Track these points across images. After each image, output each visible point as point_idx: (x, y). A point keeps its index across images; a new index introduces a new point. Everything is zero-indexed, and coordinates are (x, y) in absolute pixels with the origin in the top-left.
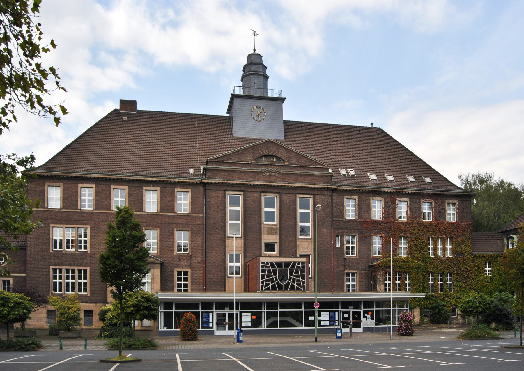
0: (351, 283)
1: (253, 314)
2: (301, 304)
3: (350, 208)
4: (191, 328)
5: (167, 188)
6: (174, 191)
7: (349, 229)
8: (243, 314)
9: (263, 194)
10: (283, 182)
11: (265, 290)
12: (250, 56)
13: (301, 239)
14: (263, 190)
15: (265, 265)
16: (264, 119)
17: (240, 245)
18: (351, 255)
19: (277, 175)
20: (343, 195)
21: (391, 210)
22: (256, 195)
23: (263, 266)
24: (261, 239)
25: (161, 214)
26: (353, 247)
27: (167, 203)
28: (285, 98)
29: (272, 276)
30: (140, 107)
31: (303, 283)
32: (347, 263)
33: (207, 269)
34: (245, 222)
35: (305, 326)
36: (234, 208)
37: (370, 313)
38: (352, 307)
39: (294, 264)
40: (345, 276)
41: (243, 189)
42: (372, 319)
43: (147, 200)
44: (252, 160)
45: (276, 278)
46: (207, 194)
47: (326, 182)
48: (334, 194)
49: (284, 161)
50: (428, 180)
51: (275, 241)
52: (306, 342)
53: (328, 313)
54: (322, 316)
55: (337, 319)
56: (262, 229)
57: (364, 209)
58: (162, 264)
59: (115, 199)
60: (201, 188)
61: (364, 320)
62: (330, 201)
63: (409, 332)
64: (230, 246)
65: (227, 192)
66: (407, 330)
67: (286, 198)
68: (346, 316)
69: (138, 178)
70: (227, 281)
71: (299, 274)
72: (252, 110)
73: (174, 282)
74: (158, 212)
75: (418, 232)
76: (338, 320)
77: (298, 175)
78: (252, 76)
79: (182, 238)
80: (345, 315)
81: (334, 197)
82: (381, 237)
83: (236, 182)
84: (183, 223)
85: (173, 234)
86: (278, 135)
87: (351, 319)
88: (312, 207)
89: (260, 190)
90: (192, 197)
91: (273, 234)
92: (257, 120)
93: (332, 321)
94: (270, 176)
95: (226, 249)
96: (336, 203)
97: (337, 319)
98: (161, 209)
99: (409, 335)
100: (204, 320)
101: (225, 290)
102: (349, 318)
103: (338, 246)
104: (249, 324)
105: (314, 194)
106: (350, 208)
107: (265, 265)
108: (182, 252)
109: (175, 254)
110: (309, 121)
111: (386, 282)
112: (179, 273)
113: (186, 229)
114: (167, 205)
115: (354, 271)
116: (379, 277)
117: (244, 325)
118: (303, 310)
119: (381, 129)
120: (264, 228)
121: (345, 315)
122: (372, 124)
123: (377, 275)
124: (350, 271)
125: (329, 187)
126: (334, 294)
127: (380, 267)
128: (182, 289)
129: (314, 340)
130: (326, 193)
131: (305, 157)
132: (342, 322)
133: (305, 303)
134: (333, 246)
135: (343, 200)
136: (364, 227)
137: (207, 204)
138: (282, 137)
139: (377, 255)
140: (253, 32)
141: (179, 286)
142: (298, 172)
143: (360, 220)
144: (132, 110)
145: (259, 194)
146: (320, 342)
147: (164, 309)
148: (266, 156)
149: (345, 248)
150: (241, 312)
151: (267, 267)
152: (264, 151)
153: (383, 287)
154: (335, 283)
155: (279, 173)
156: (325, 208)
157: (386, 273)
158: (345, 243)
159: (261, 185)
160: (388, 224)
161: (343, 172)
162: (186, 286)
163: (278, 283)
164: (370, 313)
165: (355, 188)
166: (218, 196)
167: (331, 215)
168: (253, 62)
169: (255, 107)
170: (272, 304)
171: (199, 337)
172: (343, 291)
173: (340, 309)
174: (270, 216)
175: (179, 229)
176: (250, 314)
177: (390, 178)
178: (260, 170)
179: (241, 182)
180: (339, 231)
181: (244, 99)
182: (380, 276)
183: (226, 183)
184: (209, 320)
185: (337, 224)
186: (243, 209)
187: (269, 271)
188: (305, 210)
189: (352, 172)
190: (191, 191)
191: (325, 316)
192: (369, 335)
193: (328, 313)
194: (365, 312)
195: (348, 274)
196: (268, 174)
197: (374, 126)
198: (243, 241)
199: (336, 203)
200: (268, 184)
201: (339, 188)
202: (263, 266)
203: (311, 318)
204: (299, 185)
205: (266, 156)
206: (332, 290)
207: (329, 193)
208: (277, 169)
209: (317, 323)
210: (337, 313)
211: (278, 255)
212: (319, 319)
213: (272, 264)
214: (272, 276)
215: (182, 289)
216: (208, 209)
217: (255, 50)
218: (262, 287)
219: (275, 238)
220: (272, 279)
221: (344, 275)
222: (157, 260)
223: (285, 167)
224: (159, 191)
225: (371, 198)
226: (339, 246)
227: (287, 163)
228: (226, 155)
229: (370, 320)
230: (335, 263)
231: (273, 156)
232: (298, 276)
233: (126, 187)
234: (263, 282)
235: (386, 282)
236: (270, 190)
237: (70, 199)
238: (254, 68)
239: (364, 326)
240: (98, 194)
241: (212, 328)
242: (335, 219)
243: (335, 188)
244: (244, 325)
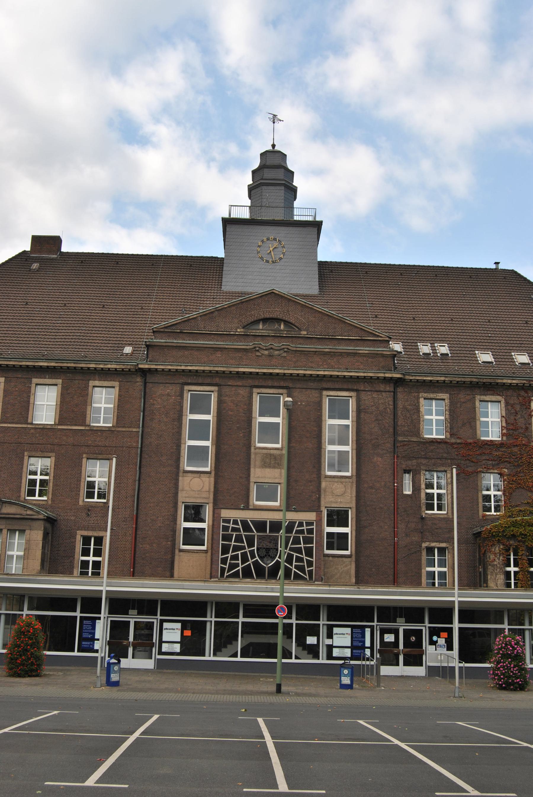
0: (437, 569)
1: (185, 625)
2: (75, 601)
3: (103, 405)
4: (26, 650)
5: (75, 380)
6: (87, 387)
7: (430, 458)
8: (166, 625)
9: (255, 390)
10: (296, 367)
11: (228, 577)
12: (263, 155)
13: (331, 477)
14: (256, 384)
15: (231, 525)
16: (280, 259)
17: (206, 488)
18: (436, 511)
19: (285, 355)
20: (419, 392)
21: (521, 422)
22: (243, 392)
23: (225, 528)
24: (249, 475)
25: (59, 427)
26: (439, 495)
27: (73, 407)
28: (322, 222)
29: (244, 548)
31: (310, 564)
33: (139, 532)
34: (218, 443)
35: (78, 651)
36: (199, 417)
37: (445, 635)
38: (403, 620)
39: (291, 525)
40: (424, 553)
41: (217, 380)
42: (450, 647)
43: (37, 403)
44: (238, 328)
45: (252, 552)
46: (147, 390)
47: (383, 367)
48: (400, 389)
49: (300, 330)
51: (277, 481)
52: (252, 693)
53: (349, 630)
54: (334, 636)
55: (368, 644)
56: (253, 456)
57: (462, 419)
58: (50, 521)
59: (482, 419)
60: (139, 379)
61: (431, 649)
62: (391, 403)
63: (513, 684)
64: (187, 488)
65: (186, 388)
66: (509, 677)
67: (305, 397)
68: (389, 638)
69: (24, 363)
70: (177, 558)
71: (302, 546)
72: (260, 243)
73: (73, 557)
74: (55, 424)
76: (372, 648)
77: (325, 354)
78: (264, 188)
79: (99, 473)
80: (386, 636)
81: (400, 396)
82: (501, 474)
83: (202, 368)
84: (100, 444)
85: (80, 465)
86: (312, 287)
87: (401, 646)
88: (355, 414)
89: (250, 382)
90: (120, 396)
91: (274, 467)
92: (267, 261)
93: (357, 647)
94: (270, 356)
95: (180, 495)
96: (404, 408)
97: (368, 644)
99: (515, 690)
100: (85, 635)
101: (172, 576)
102: (396, 644)
103: (408, 491)
104: (177, 648)
105: (357, 390)
106: (103, 405)
107: (231, 525)
108: (96, 500)
109: (81, 503)
110: (397, 263)
111: (508, 569)
112: (86, 540)
113: (104, 456)
114: (73, 411)
115: (443, 545)
116: (492, 557)
117: (165, 648)
118: (78, 614)
119: (516, 272)
120: (256, 454)
121: (386, 636)
122: (497, 263)
123: (488, 554)
124: (433, 544)
125: (387, 375)
126: (362, 589)
127: (493, 536)
128: (90, 570)
129: (274, 688)
130: (382, 387)
131: (342, 321)
132: (380, 651)
133: (83, 599)
134: (397, 491)
135: (418, 402)
137: (147, 409)
138: (314, 289)
139: (493, 513)
140: (271, 116)
141: (85, 564)
142: (326, 348)
143: (453, 441)
144: (50, 252)
145: (248, 389)
146: (288, 694)
147: (328, 620)
148: (265, 320)
149: (423, 496)
150: (162, 622)
151: (234, 529)
152: (269, 312)
153: (501, 578)
154: (401, 567)
155: (288, 351)
156: (380, 418)
157: (508, 550)
158: (423, 486)
159: (251, 373)
160: (515, 449)
161: (425, 349)
162: (97, 565)
163: (256, 563)
164: (445, 635)
165: (443, 379)
166: (168, 395)
167: (391, 430)
168: (268, 164)
169: (265, 239)
170: (227, 607)
171: (46, 669)
172: (418, 584)
173: (375, 623)
174: (269, 431)
175: (91, 456)
176: (179, 625)
177: (522, 358)
178: (250, 345)
179: (211, 369)
180: (409, 463)
181: (246, 226)
182: (495, 554)
183: (183, 370)
184: (364, 642)
185: (406, 448)
186: (215, 419)
187: (239, 539)
188: (338, 435)
189: (444, 349)
190: (120, 386)
191: (342, 637)
192: (440, 684)
193: (349, 630)
194: (434, 632)
195: (430, 551)
196: (266, 352)
197: (501, 267)
198: (212, 479)
199: (404, 408)
200: (265, 371)
201: (407, 377)
202: (225, 528)
203: (311, 640)
204: (326, 373)
205: (265, 320)
206: (395, 582)
207: (390, 387)
208: (284, 343)
209: (323, 652)
210: (368, 632)
211: (284, 508)
212: (329, 642)
213: (245, 523)
214: (244, 548)
215: (90, 570)
216: (147, 419)
217: (274, 146)
218: (223, 570)
219: (277, 475)
220: (244, 555)
221: (420, 551)
222: (38, 513)
223: (301, 341)
224: (60, 386)
225: (478, 397)
226: (410, 493)
227: (305, 333)
228: (188, 320)
229: (444, 651)
230: (401, 526)
231: (278, 320)
232: (299, 550)
233: (116, 384)
234: (224, 561)
235: (508, 569)
236: (270, 383)
238: (268, 174)
239: (428, 664)
241: (97, 651)
242: (400, 439)
243: (401, 378)
244: (165, 648)
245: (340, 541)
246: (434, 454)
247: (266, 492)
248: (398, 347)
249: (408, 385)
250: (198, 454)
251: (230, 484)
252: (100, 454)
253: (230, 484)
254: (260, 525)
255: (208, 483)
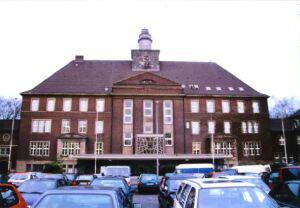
27: (75, 106)
30: (85, 59)
32: (193, 136)
36: (128, 107)
50: (241, 89)
57: (203, 106)
75: (236, 120)
98: (89, 110)
134: (185, 126)
136: (203, 118)
142: (163, 87)
177: (219, 89)
188: (168, 108)
189: (196, 86)
237: (43, 106)
240: (89, 103)
245: (169, 142)
246: (194, 117)
247: (148, 129)
248: (183, 86)
249: (186, 97)
250: (128, 119)
251: (138, 126)
252: (83, 119)
253: (138, 126)
254: (148, 139)
255: (131, 127)
